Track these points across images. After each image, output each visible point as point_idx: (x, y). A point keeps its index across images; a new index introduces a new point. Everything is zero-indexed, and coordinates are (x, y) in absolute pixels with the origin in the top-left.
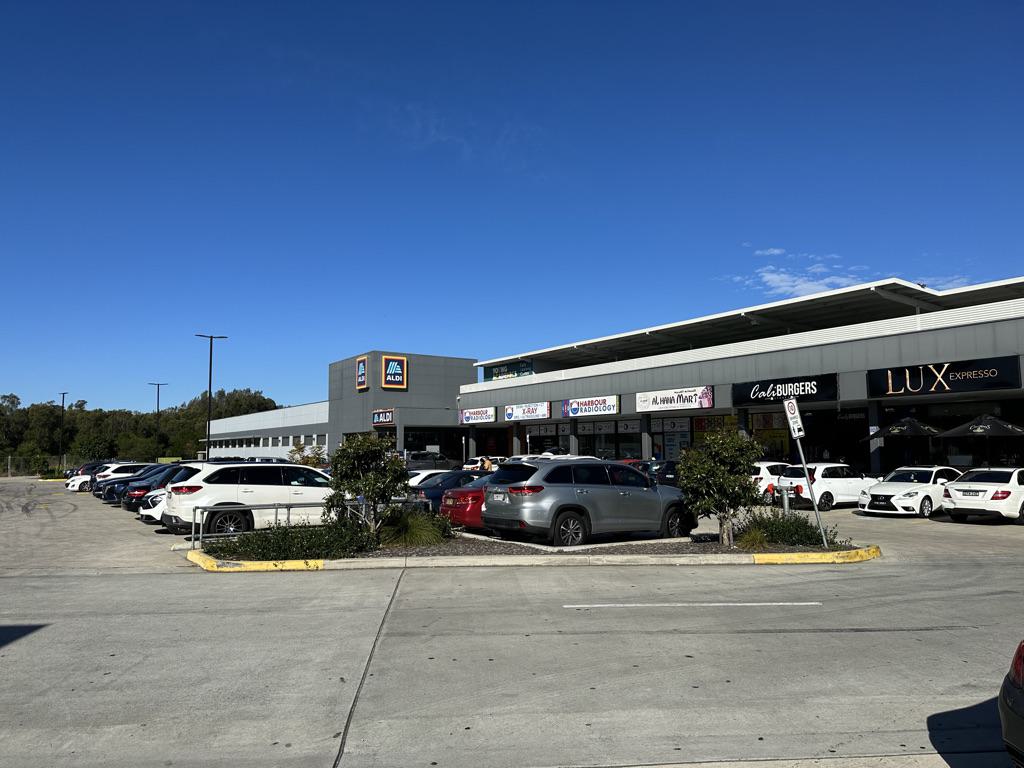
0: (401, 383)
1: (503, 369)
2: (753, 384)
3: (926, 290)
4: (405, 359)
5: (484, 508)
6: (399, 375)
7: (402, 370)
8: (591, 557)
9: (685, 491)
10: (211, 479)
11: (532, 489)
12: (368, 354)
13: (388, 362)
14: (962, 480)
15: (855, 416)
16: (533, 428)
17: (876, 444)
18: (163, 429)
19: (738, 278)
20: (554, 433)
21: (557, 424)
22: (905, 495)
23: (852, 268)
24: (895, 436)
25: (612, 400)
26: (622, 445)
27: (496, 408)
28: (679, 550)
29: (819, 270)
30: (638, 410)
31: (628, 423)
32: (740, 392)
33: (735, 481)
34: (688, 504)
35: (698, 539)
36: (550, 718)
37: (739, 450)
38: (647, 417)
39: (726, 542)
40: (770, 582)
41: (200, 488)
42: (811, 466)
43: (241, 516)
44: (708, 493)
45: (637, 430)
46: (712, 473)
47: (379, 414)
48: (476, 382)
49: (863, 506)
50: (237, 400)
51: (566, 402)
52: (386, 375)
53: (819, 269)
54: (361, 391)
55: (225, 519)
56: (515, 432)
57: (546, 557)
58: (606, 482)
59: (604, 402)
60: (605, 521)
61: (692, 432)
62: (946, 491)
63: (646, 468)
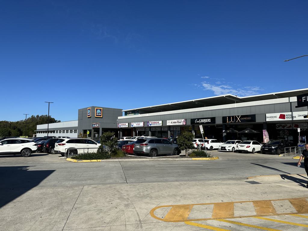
0: (101, 116)
1: (131, 112)
2: (196, 119)
3: (237, 97)
4: (102, 109)
5: (134, 149)
6: (100, 113)
7: (101, 112)
8: (159, 159)
9: (178, 145)
10: (68, 142)
11: (145, 144)
12: (91, 107)
13: (97, 109)
14: (241, 143)
15: (220, 127)
16: (139, 129)
17: (224, 134)
18: (19, 127)
19: (196, 85)
20: (144, 130)
21: (145, 128)
22: (229, 147)
23: (228, 83)
24: (228, 133)
25: (161, 122)
26: (162, 134)
27: (129, 123)
28: (177, 157)
29: (219, 83)
30: (167, 125)
31: (164, 128)
32: (193, 121)
33: (189, 143)
34: (179, 148)
35: (180, 156)
36: (157, 178)
37: (190, 136)
38: (170, 126)
39: (187, 156)
40: (195, 162)
41: (65, 144)
42: (208, 140)
43: (74, 151)
44: (183, 145)
45: (167, 130)
46: (184, 141)
47: (94, 124)
48: (122, 116)
49: (219, 149)
50: (43, 118)
51: (148, 122)
52: (96, 113)
53: (219, 83)
54: (88, 118)
55: (71, 151)
56: (134, 130)
57: (149, 159)
58: (162, 143)
59: (158, 122)
60: (161, 152)
61: (181, 131)
62: (237, 146)
63: (169, 140)
